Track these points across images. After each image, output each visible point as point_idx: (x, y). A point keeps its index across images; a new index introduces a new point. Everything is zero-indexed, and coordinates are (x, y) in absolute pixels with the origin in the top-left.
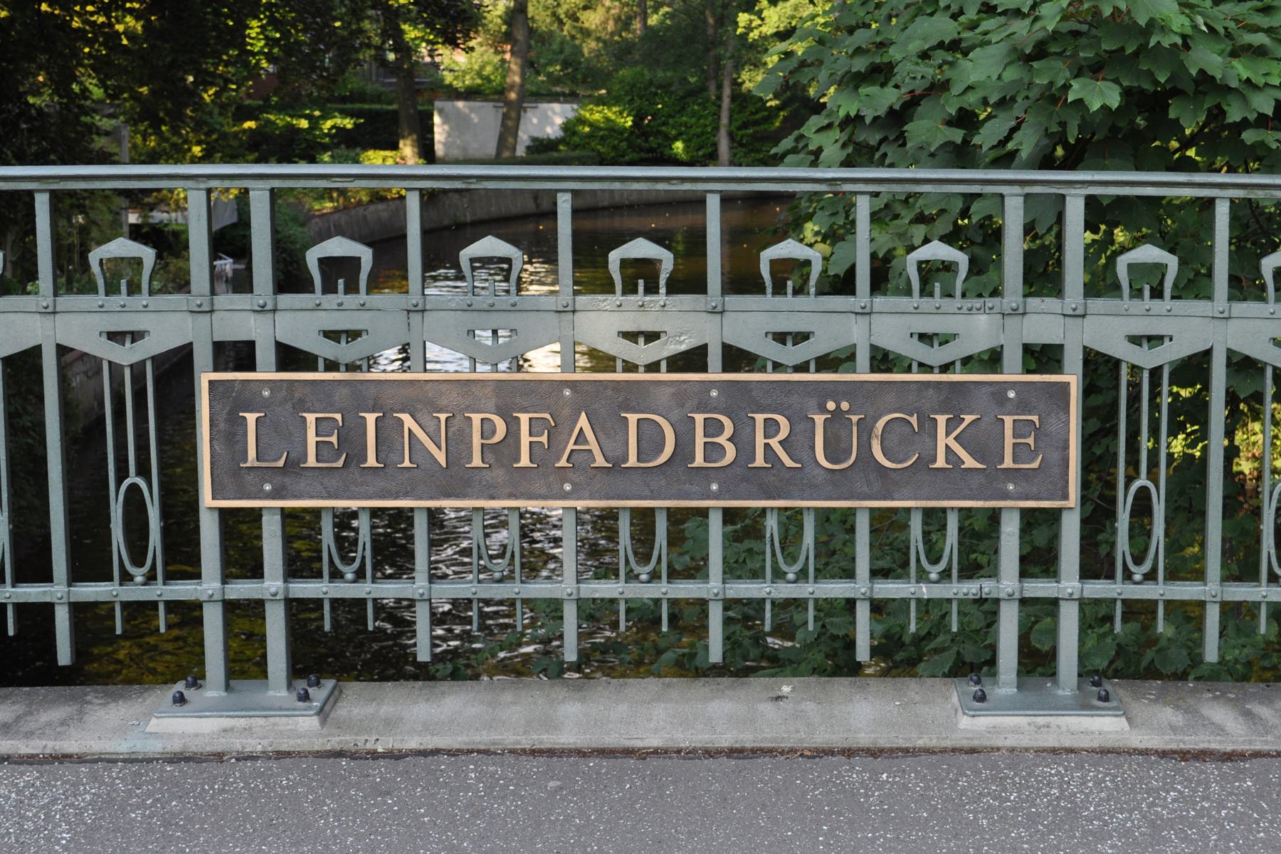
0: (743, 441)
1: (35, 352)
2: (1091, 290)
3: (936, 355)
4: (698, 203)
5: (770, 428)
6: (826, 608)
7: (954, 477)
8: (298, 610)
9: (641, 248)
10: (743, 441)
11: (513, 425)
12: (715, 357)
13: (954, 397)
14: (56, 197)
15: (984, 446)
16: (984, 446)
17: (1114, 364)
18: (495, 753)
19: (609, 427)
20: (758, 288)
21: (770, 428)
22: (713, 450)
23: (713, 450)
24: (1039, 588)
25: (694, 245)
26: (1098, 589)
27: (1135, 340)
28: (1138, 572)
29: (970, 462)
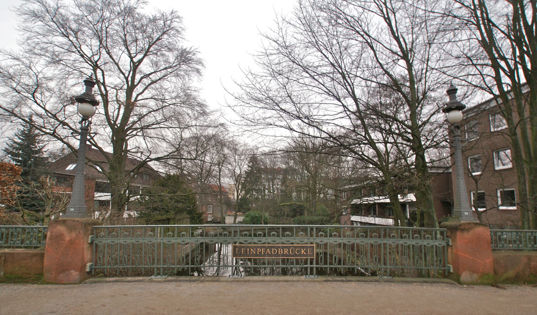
0: (283, 251)
1: (354, 243)
2: (316, 237)
3: (302, 243)
4: (265, 229)
5: (286, 250)
6: (325, 268)
7: (304, 255)
8: (317, 268)
9: (274, 233)
10: (283, 251)
11: (262, 250)
12: (253, 243)
13: (303, 247)
14: (316, 228)
15: (306, 252)
16: (306, 252)
17: (208, 244)
18: (322, 281)
19: (271, 251)
20: (257, 236)
21: (286, 250)
22: (281, 252)
23: (281, 252)
24: (312, 266)
25: (278, 233)
26: (318, 266)
27: (348, 242)
28: (321, 264)
29: (305, 253)
